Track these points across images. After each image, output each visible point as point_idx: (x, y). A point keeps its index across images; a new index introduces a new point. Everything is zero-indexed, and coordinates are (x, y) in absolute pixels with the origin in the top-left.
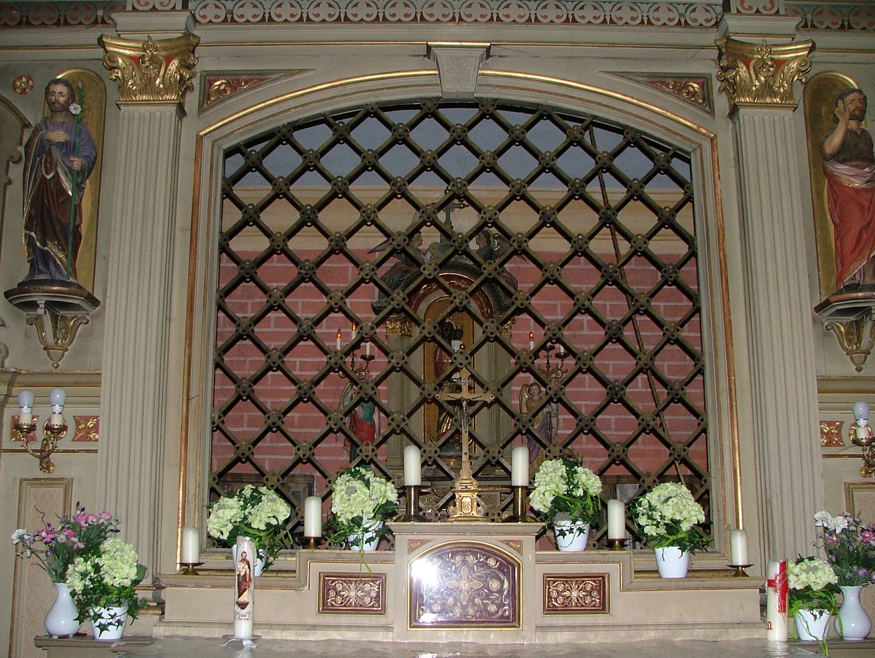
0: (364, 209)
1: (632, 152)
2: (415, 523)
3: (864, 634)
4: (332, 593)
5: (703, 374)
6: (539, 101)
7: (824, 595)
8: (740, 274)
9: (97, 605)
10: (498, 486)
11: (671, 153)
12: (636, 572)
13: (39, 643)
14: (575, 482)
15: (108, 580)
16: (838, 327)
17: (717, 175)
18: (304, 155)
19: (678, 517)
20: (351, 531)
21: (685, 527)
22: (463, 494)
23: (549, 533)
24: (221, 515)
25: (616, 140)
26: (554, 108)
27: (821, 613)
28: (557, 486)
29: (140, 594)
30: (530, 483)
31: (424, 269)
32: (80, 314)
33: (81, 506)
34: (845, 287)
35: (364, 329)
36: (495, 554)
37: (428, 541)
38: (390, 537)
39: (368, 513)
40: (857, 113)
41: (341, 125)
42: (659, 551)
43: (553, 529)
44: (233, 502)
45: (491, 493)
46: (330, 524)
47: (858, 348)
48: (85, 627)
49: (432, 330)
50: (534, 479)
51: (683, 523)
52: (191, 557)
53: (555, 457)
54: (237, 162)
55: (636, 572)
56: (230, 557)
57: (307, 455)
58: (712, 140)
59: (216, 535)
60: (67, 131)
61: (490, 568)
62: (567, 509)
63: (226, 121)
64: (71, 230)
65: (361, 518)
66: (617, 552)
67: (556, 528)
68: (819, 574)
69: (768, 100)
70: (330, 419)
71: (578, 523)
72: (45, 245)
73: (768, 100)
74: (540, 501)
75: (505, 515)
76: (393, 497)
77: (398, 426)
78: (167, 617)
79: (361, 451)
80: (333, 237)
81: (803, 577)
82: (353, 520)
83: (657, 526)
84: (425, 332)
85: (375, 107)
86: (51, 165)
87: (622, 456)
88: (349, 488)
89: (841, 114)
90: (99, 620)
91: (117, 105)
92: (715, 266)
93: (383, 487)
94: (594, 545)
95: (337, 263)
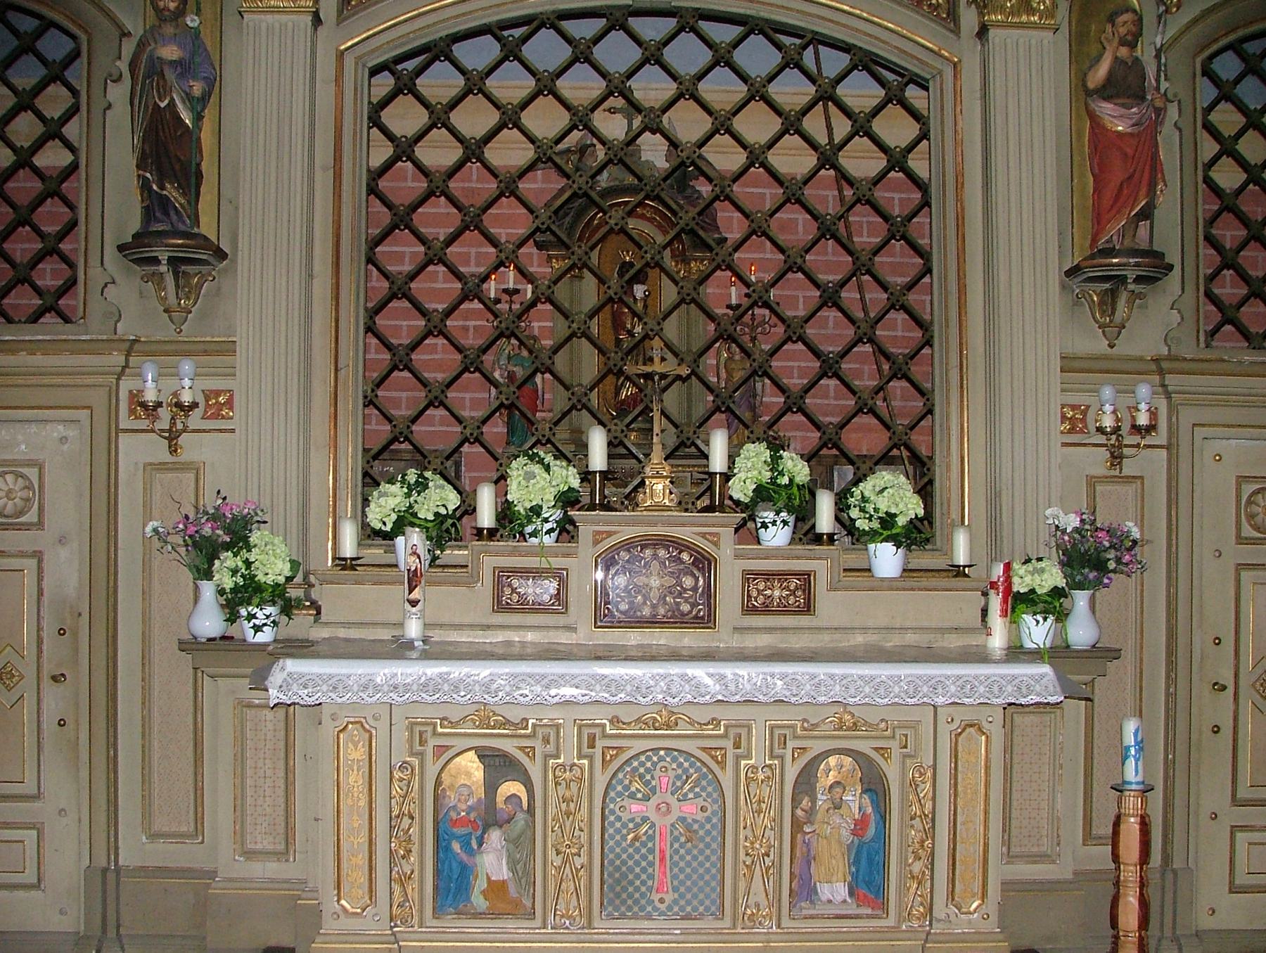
0: (538, 144)
1: (860, 77)
2: (602, 513)
3: (1092, 642)
4: (507, 591)
5: (931, 346)
6: (749, 12)
7: (1049, 599)
8: (980, 267)
9: (249, 604)
10: (689, 466)
11: (905, 80)
12: (845, 570)
13: (184, 646)
14: (780, 469)
15: (261, 577)
16: (1091, 296)
17: (958, 110)
18: (467, 76)
19: (893, 511)
20: (530, 522)
21: (901, 521)
22: (654, 481)
23: (750, 525)
24: (383, 504)
25: (844, 60)
26: (767, 21)
27: (1045, 619)
28: (760, 473)
29: (293, 593)
30: (729, 468)
31: (610, 217)
32: (204, 269)
33: (223, 494)
34: (1099, 251)
35: (540, 287)
36: (688, 548)
37: (615, 533)
38: (570, 528)
39: (549, 501)
40: (1129, 38)
41: (511, 39)
42: (872, 546)
43: (754, 520)
44: (395, 488)
45: (680, 474)
46: (505, 513)
47: (1111, 321)
48: (233, 631)
49: (619, 290)
50: (734, 463)
51: (900, 517)
52: (349, 548)
53: (758, 439)
54: (385, 83)
55: (845, 570)
56: (392, 550)
57: (475, 435)
58: (955, 65)
59: (378, 526)
60: (180, 46)
61: (684, 563)
62: (770, 499)
63: (371, 32)
64: (193, 170)
65: (541, 507)
66: (825, 547)
67: (758, 519)
68: (1045, 576)
69: (1024, 18)
70: (501, 393)
71: (782, 514)
72: (162, 188)
73: (1024, 18)
74: (741, 489)
75: (700, 504)
76: (575, 483)
77: (579, 401)
78: (324, 618)
79: (537, 429)
80: (501, 177)
81: (1028, 579)
82: (532, 509)
83: (870, 520)
84: (611, 292)
85: (552, 17)
86: (164, 90)
87: (835, 438)
88: (526, 473)
89: (1109, 41)
90: (254, 621)
91: (240, 12)
92: (951, 216)
93: (565, 472)
94: (800, 539)
95: (507, 207)
